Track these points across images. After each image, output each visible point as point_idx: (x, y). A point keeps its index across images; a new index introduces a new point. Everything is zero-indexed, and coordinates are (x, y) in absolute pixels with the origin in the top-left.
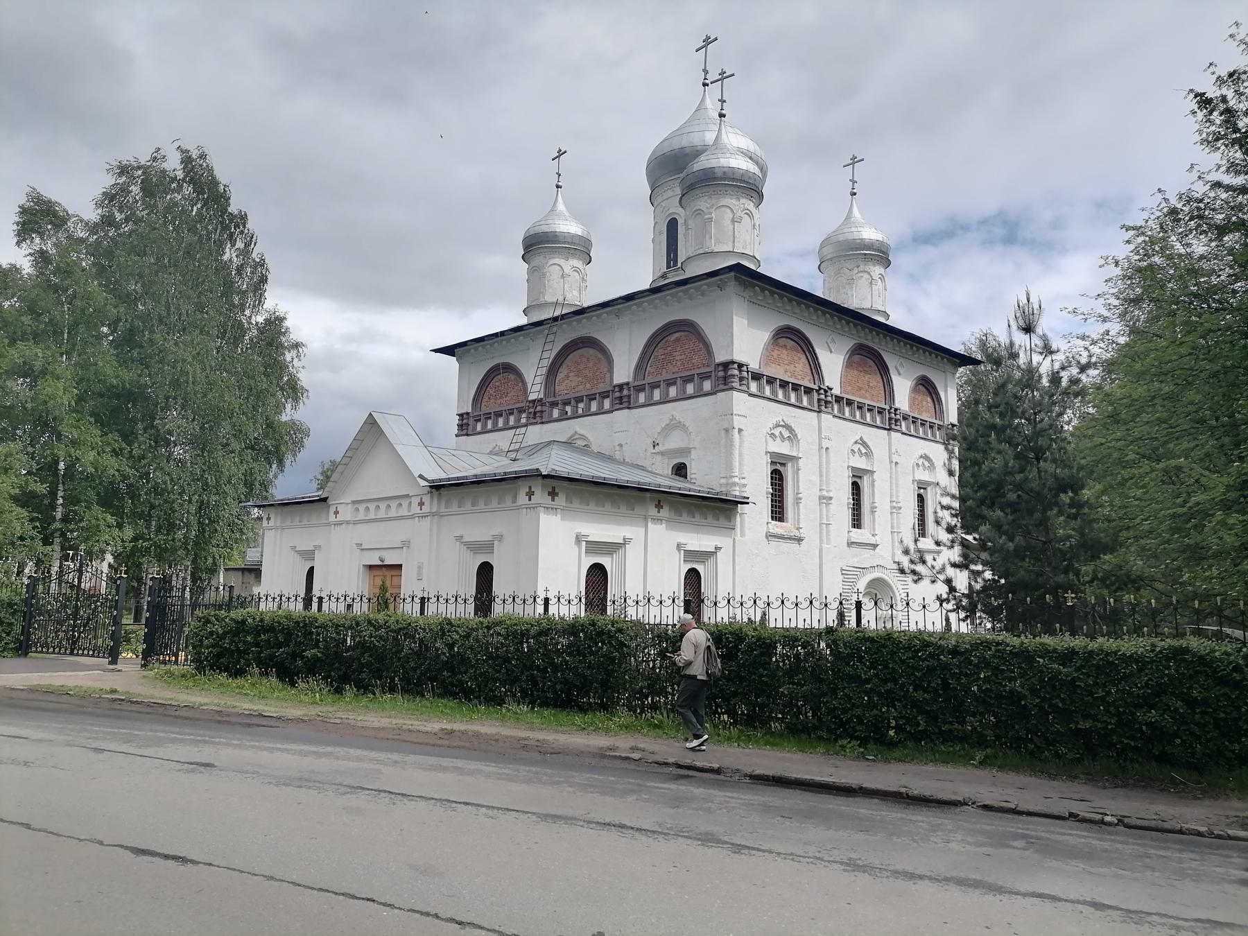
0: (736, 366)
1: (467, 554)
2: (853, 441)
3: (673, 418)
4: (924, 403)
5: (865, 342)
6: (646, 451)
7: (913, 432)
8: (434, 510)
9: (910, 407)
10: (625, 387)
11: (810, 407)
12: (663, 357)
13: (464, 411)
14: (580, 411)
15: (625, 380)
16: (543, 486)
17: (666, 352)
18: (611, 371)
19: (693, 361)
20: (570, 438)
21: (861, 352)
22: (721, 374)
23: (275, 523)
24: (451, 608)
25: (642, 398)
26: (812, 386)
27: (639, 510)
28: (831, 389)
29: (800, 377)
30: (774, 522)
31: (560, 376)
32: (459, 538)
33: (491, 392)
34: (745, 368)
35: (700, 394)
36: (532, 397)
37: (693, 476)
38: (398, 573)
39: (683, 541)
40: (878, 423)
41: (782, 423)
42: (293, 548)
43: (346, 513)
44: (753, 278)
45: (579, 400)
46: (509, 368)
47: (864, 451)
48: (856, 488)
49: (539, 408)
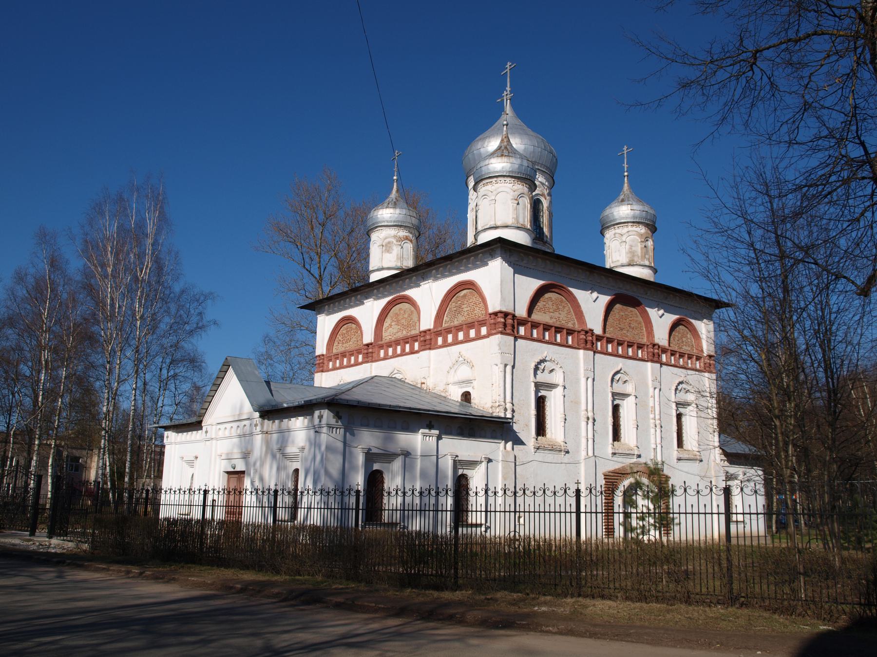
0: (502, 315)
4: (684, 339)
5: (623, 291)
12: (455, 309)
24: (539, 500)
31: (386, 325)
35: (479, 337)
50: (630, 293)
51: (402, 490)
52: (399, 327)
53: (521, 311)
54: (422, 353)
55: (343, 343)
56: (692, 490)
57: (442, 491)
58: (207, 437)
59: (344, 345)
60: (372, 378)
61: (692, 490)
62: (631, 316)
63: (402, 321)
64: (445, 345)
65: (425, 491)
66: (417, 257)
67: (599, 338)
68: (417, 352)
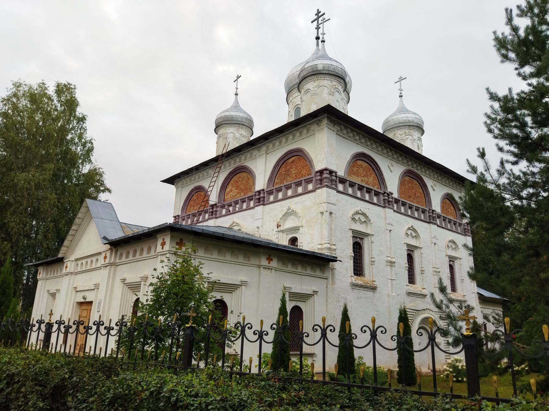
0: (328, 172)
2: (407, 227)
4: (449, 210)
6: (273, 230)
7: (444, 226)
9: (442, 212)
10: (262, 192)
11: (378, 204)
12: (284, 173)
13: (177, 214)
14: (237, 209)
15: (262, 188)
17: (286, 169)
18: (254, 184)
20: (231, 225)
21: (410, 175)
22: (319, 178)
23: (43, 275)
25: (272, 198)
26: (379, 191)
27: (254, 261)
28: (392, 194)
29: (371, 185)
30: (355, 277)
31: (228, 190)
33: (192, 203)
34: (334, 174)
36: (211, 203)
37: (301, 244)
38: (89, 308)
39: (286, 285)
40: (422, 218)
41: (360, 212)
42: (48, 291)
44: (339, 119)
45: (236, 203)
46: (199, 189)
47: (414, 234)
48: (410, 258)
49: (215, 209)
52: (238, 191)
54: (256, 208)
55: (194, 207)
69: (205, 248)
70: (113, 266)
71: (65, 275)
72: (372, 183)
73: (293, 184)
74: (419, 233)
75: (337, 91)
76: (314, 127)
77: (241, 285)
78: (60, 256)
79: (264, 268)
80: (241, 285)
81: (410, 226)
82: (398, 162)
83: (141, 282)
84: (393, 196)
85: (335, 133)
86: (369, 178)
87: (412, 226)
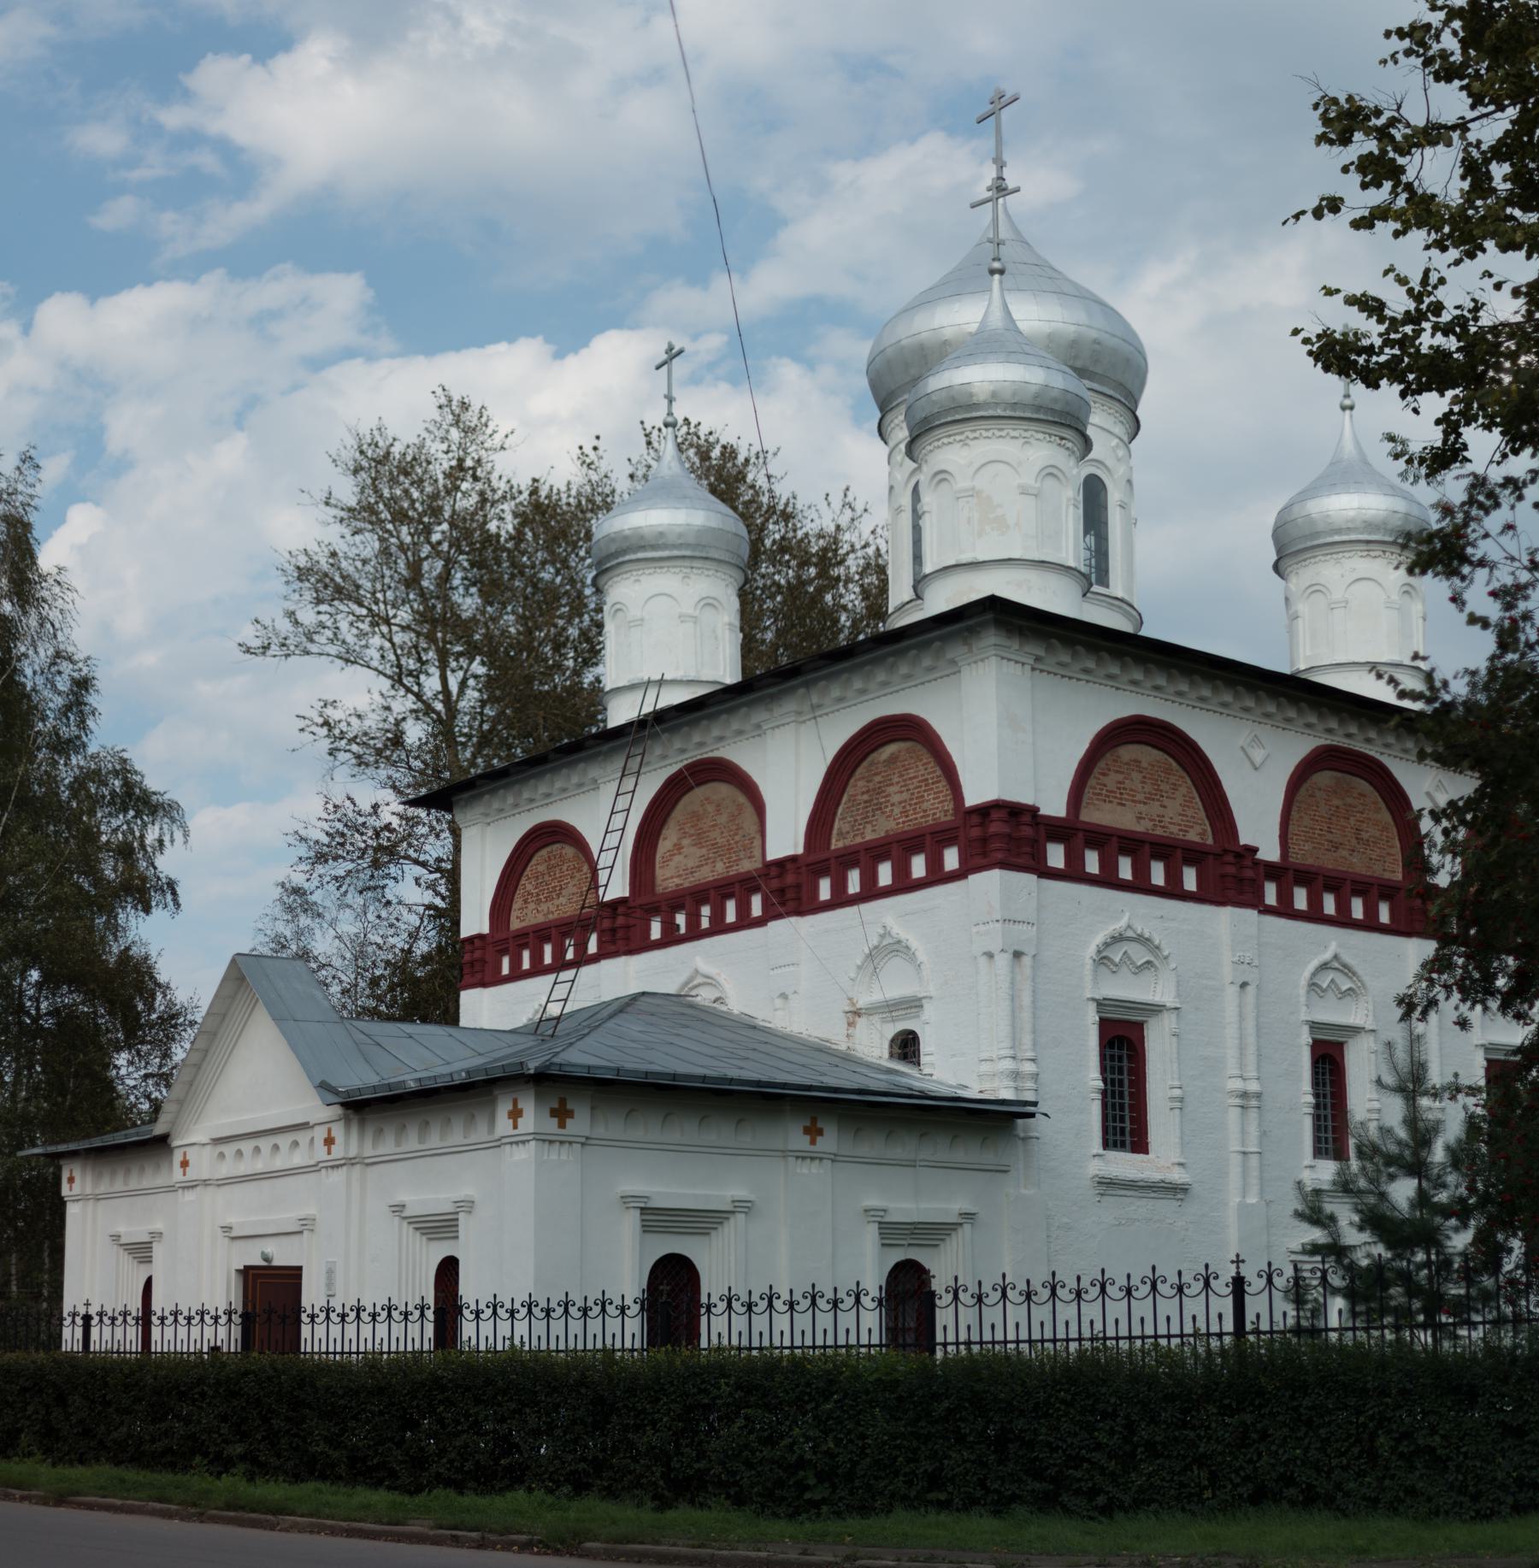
0: (1002, 814)
1: (416, 1240)
3: (886, 934)
8: (353, 1152)
10: (789, 866)
12: (866, 797)
15: (789, 852)
16: (539, 1097)
17: (871, 785)
19: (925, 805)
20: (686, 984)
22: (975, 832)
31: (664, 846)
32: (398, 1209)
33: (529, 887)
41: (1130, 934)
43: (203, 1164)
49: (620, 920)
50: (1359, 746)
51: (473, 1307)
52: (704, 851)
53: (1054, 805)
54: (774, 926)
55: (539, 902)
56: (1066, 1290)
57: (1192, 1282)
58: (187, 1178)
59: (544, 907)
60: (635, 998)
61: (1066, 1290)
62: (1361, 808)
63: (712, 835)
64: (841, 900)
65: (800, 1299)
66: (749, 648)
67: (1272, 871)
68: (760, 922)
69: (627, 1115)
70: (358, 1166)
71: (183, 1188)
72: (1177, 819)
73: (895, 845)
74: (1365, 978)
75: (1051, 474)
76: (956, 651)
77: (733, 1212)
78: (159, 1129)
79: (797, 1157)
80: (733, 1212)
81: (1327, 956)
82: (1265, 732)
83: (457, 1213)
84: (1260, 855)
85: (1028, 668)
86: (1166, 802)
87: (1336, 957)
